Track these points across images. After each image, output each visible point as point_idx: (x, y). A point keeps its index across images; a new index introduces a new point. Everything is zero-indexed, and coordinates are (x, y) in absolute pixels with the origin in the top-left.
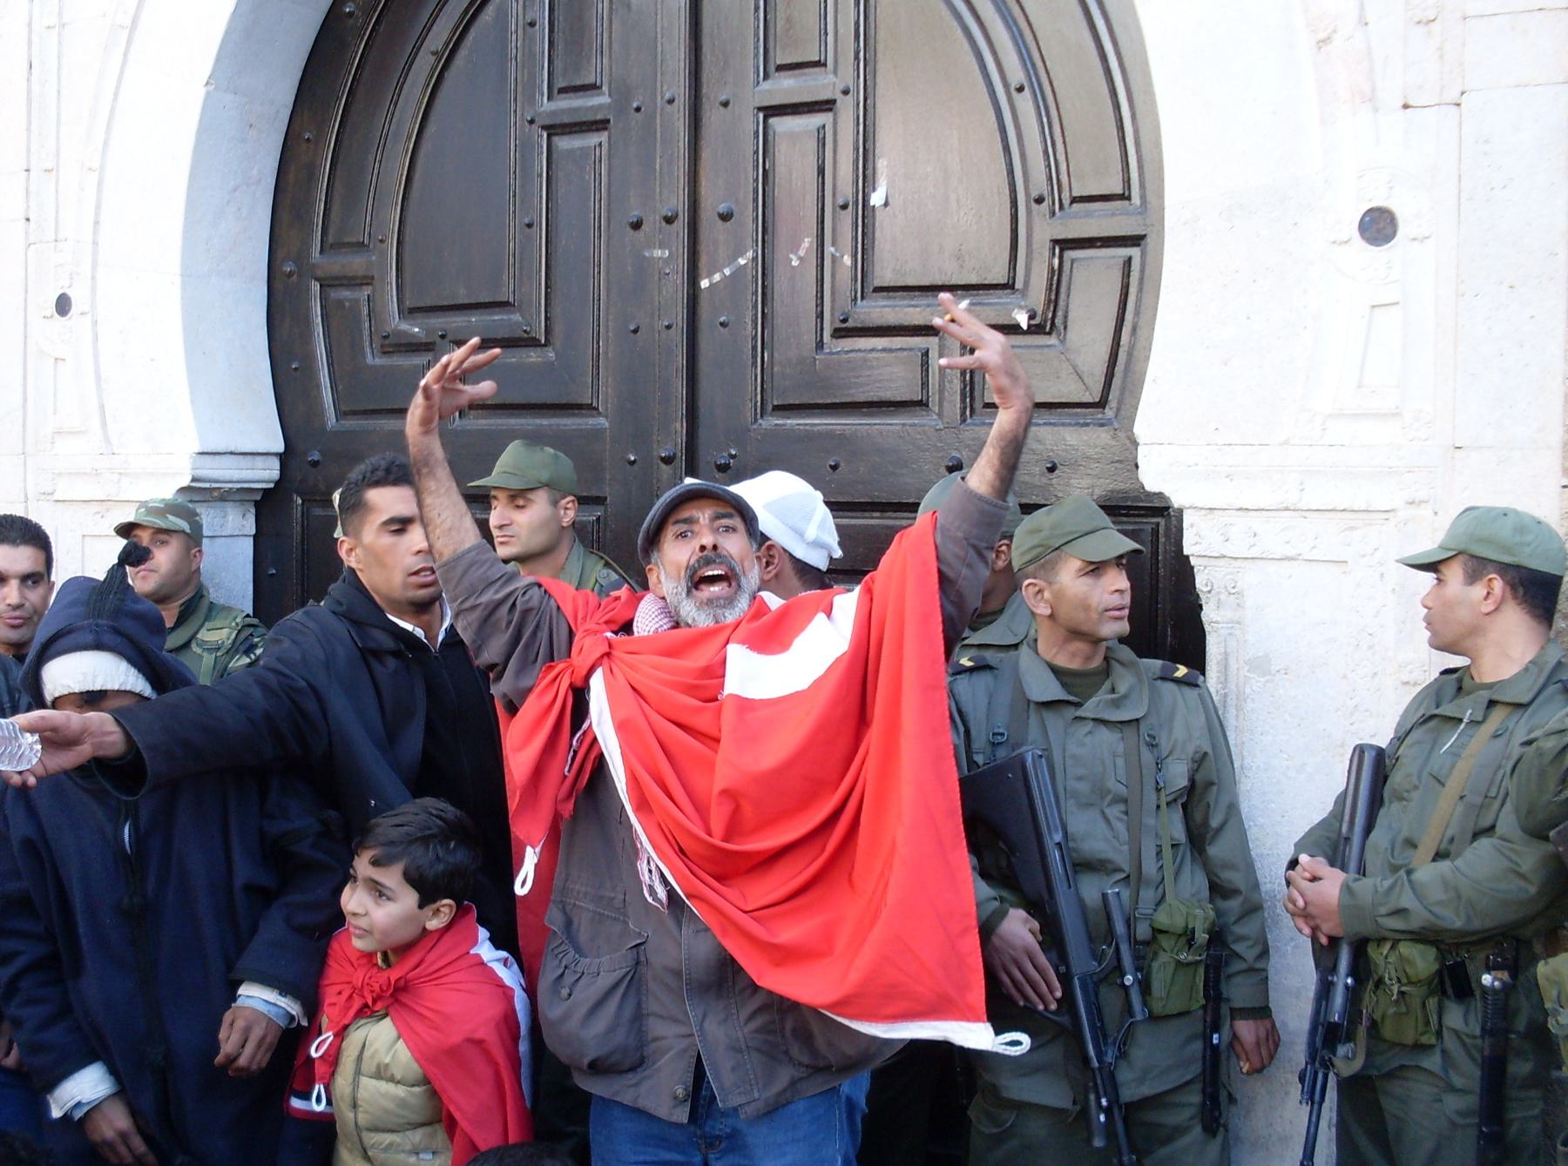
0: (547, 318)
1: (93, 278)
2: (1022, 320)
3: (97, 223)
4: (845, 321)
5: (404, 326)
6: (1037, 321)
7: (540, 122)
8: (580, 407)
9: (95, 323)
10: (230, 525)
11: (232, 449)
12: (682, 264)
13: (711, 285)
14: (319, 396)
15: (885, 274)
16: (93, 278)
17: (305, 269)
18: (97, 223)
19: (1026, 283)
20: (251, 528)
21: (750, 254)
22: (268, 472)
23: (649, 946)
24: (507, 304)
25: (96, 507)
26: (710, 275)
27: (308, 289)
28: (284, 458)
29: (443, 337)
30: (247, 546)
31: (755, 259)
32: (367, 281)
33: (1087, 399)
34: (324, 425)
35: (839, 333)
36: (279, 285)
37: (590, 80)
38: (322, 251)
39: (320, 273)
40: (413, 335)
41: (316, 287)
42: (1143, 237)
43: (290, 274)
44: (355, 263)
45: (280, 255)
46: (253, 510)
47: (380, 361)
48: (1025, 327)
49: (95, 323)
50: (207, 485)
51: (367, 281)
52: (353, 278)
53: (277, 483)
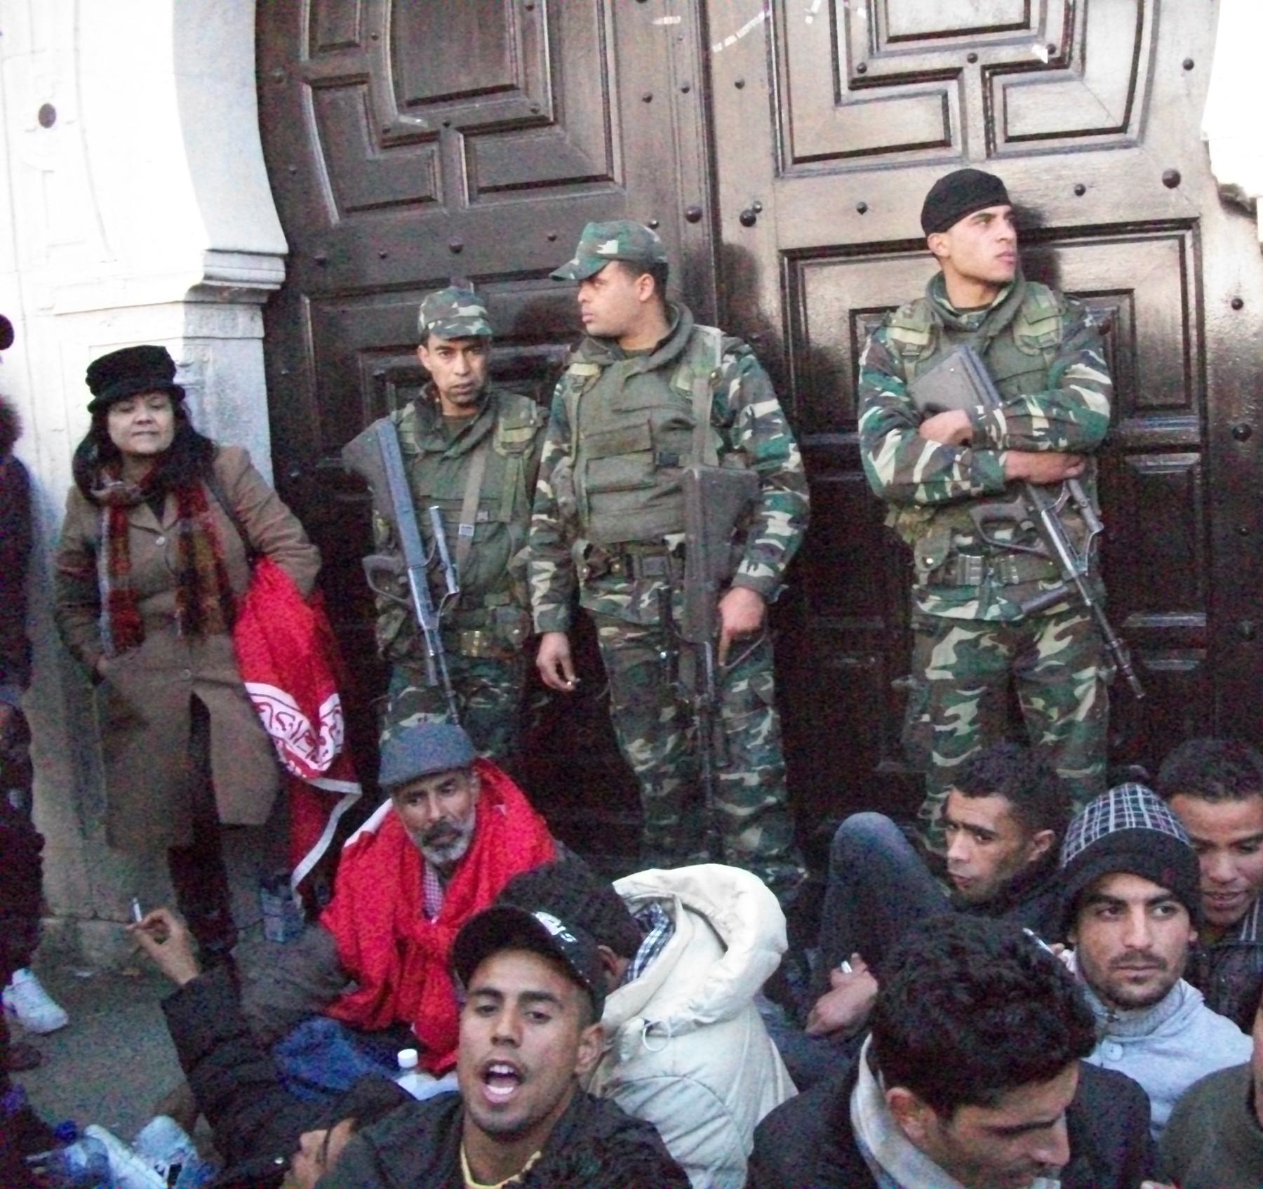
0: (554, 98)
1: (78, 85)
2: (1044, 56)
3: (76, 29)
4: (863, 70)
5: (405, 119)
6: (1057, 54)
7: (456, 124)
8: (595, 179)
9: (84, 131)
10: (241, 327)
11: (240, 247)
12: (693, 26)
13: (725, 48)
14: (320, 196)
15: (901, 25)
16: (78, 85)
17: (295, 76)
18: (76, 29)
19: (1043, 21)
20: (259, 331)
21: (762, 16)
22: (274, 273)
23: (762, 213)
24: (511, 88)
25: (100, 316)
26: (722, 40)
27: (300, 95)
28: (289, 260)
29: (447, 125)
30: (256, 352)
31: (767, 19)
32: (362, 79)
33: (1109, 124)
34: (327, 221)
35: (855, 85)
36: (268, 95)
37: (507, 82)
38: (312, 55)
39: (312, 76)
40: (415, 126)
41: (308, 90)
42: (1195, 220)
43: (280, 80)
44: (348, 65)
45: (268, 62)
46: (260, 313)
47: (380, 156)
48: (1046, 61)
49: (84, 131)
50: (218, 284)
51: (362, 79)
52: (350, 76)
53: (284, 285)
